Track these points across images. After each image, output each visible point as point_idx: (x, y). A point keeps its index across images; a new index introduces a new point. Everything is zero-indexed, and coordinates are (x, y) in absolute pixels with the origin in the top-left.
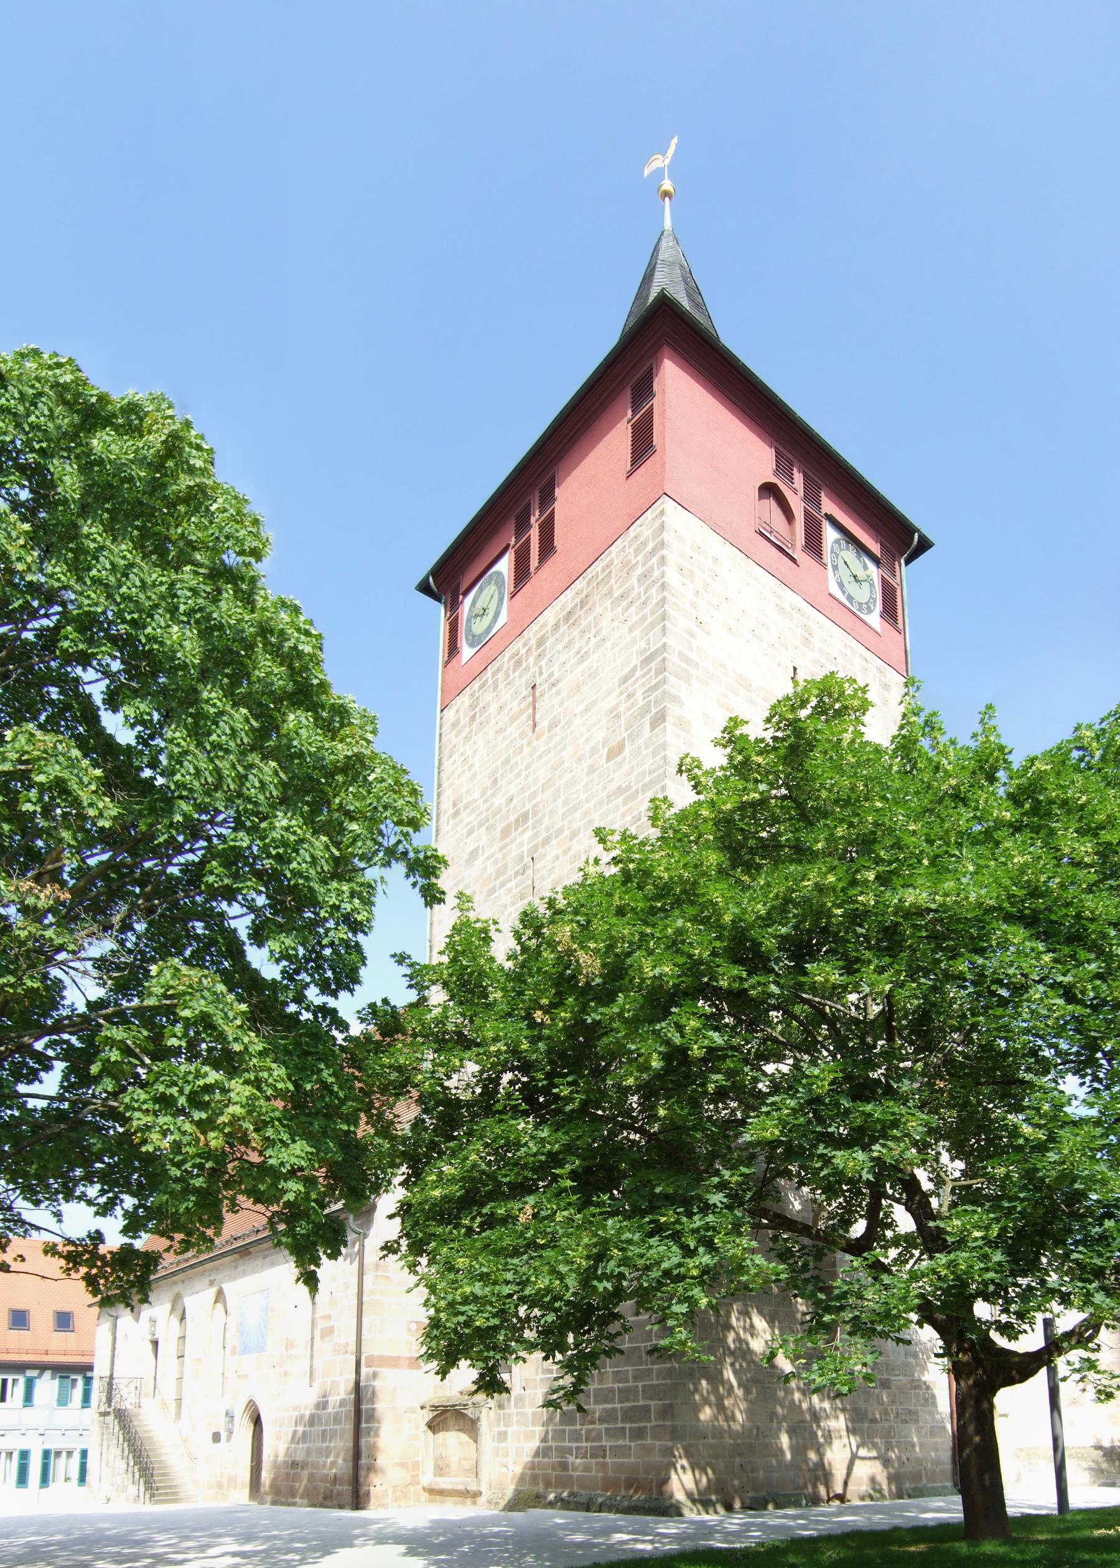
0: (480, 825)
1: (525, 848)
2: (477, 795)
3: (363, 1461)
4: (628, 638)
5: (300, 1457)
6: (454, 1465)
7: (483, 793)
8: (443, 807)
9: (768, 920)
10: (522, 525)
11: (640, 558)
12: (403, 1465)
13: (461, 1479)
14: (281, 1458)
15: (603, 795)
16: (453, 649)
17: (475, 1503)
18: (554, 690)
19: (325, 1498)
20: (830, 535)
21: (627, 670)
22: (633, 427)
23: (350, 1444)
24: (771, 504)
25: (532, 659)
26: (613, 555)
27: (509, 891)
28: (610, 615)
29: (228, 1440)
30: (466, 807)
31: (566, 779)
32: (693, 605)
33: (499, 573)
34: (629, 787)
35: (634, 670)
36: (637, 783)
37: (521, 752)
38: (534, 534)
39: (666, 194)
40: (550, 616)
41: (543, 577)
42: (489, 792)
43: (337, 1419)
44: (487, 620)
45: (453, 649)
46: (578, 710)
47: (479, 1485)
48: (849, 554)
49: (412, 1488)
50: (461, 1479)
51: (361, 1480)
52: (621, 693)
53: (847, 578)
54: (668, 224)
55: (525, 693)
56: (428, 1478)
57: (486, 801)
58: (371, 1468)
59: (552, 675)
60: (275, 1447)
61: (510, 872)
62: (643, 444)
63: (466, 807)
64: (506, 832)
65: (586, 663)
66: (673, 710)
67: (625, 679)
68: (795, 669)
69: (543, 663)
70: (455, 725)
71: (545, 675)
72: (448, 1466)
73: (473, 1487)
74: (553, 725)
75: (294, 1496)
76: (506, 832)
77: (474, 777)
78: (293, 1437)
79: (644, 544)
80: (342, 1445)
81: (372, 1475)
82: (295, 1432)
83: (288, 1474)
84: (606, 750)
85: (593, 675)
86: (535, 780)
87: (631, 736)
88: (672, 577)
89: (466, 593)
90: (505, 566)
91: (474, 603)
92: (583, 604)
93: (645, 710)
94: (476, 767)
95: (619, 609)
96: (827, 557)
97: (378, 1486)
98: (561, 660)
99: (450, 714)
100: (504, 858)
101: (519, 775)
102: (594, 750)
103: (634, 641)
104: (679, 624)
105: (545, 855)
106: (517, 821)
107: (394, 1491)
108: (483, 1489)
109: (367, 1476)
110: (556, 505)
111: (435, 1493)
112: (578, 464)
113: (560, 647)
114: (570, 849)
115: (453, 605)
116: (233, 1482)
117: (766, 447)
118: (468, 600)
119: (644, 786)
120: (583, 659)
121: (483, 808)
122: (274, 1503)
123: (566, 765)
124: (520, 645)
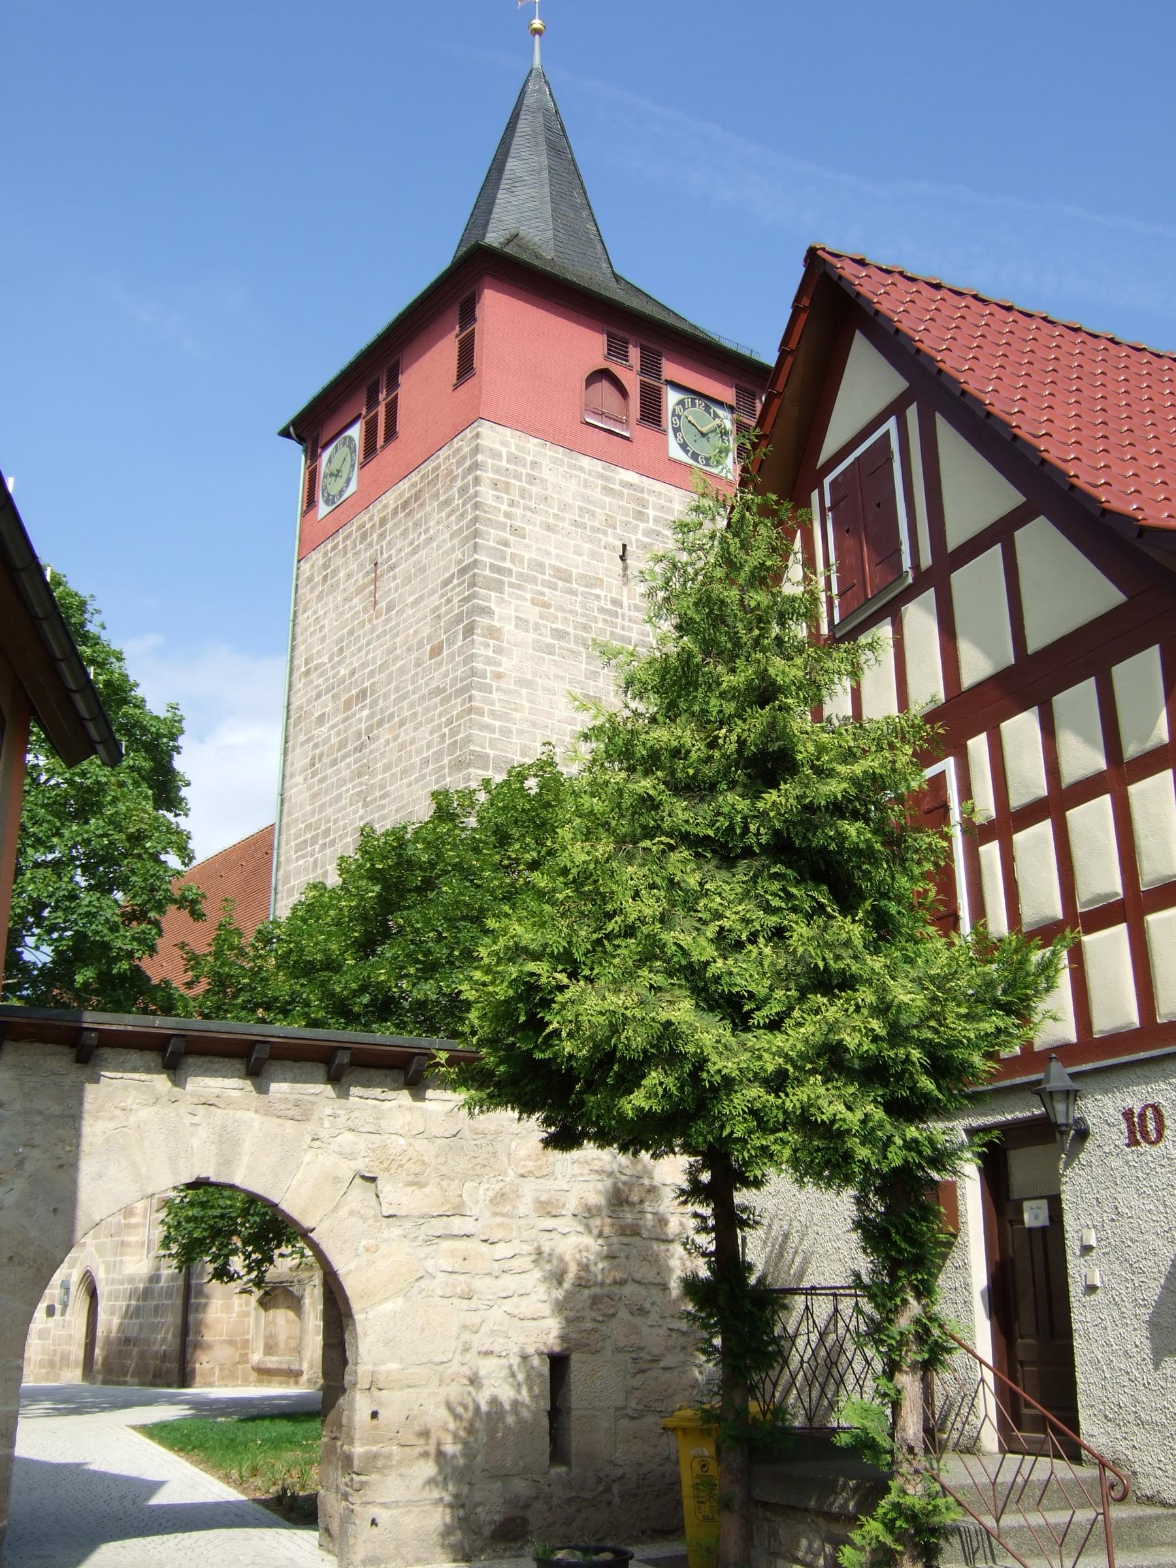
0: (328, 691)
1: (363, 726)
2: (325, 659)
3: (191, 1338)
4: (449, 545)
5: (133, 1333)
6: (282, 1345)
7: (331, 659)
8: (296, 662)
9: (356, 993)
10: (372, 402)
11: (460, 471)
12: (231, 1343)
13: (287, 1358)
14: (113, 1334)
15: (425, 691)
16: (311, 502)
17: (297, 1383)
18: (391, 574)
19: (154, 1376)
20: (672, 398)
21: (447, 575)
22: (461, 342)
23: (179, 1320)
24: (605, 386)
25: (375, 536)
26: (441, 459)
27: (349, 766)
28: (436, 517)
29: (63, 1313)
30: (316, 669)
31: (398, 665)
32: (508, 515)
33: (351, 439)
34: (445, 690)
35: (452, 577)
36: (451, 687)
37: (363, 627)
38: (381, 410)
39: (537, 32)
40: (390, 499)
41: (387, 457)
42: (336, 659)
43: (168, 1293)
44: (340, 482)
45: (311, 502)
46: (410, 600)
47: (301, 1361)
48: (696, 412)
49: (240, 1367)
50: (287, 1358)
51: (188, 1356)
52: (442, 596)
53: (688, 435)
54: (537, 61)
55: (368, 568)
56: (256, 1357)
57: (333, 667)
58: (198, 1345)
59: (390, 558)
60: (109, 1321)
61: (350, 747)
62: (466, 366)
63: (316, 669)
64: (348, 704)
65: (417, 556)
66: (482, 621)
67: (446, 583)
68: (624, 546)
69: (384, 543)
70: (310, 579)
71: (385, 556)
72: (276, 1345)
73: (295, 1367)
74: (390, 608)
75: (125, 1375)
76: (348, 704)
77: (323, 639)
78: (126, 1312)
79: (464, 458)
80: (170, 1320)
81: (198, 1352)
82: (128, 1306)
83: (120, 1351)
84: (429, 647)
85: (422, 570)
86: (374, 658)
87: (448, 639)
88: (487, 494)
89: (325, 447)
90: (356, 432)
91: (330, 461)
92: (417, 496)
93: (459, 619)
94: (326, 630)
95: (443, 514)
96: (668, 421)
97: (204, 1363)
98: (398, 546)
99: (306, 566)
100: (345, 731)
101: (360, 649)
102: (421, 645)
103: (453, 549)
104: (492, 536)
105: (378, 738)
106: (358, 696)
107: (221, 1370)
108: (305, 1367)
109: (193, 1353)
110: (399, 391)
111: (264, 1373)
112: (416, 360)
113: (398, 532)
114: (398, 736)
115: (313, 456)
116: (65, 1359)
117: (597, 335)
118: (326, 455)
119: (456, 691)
120: (415, 551)
121: (330, 674)
122: (105, 1382)
123: (398, 651)
124: (366, 518)
